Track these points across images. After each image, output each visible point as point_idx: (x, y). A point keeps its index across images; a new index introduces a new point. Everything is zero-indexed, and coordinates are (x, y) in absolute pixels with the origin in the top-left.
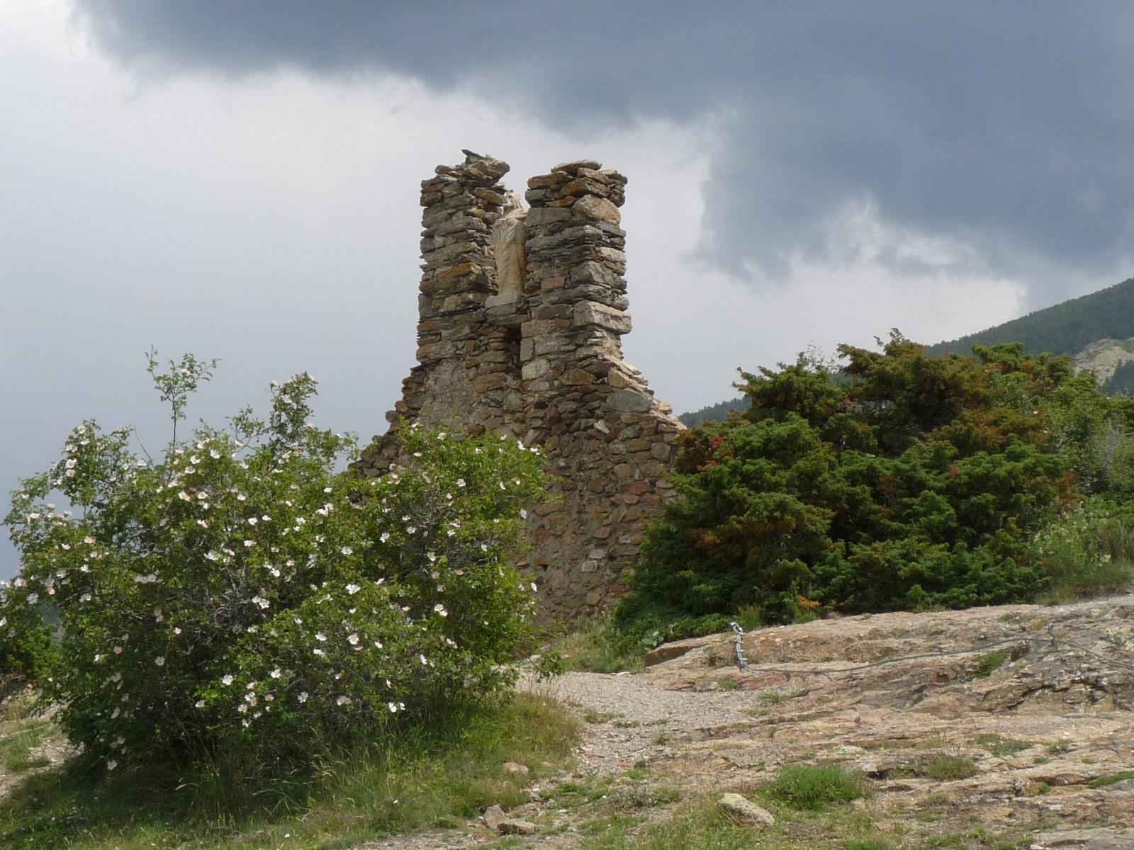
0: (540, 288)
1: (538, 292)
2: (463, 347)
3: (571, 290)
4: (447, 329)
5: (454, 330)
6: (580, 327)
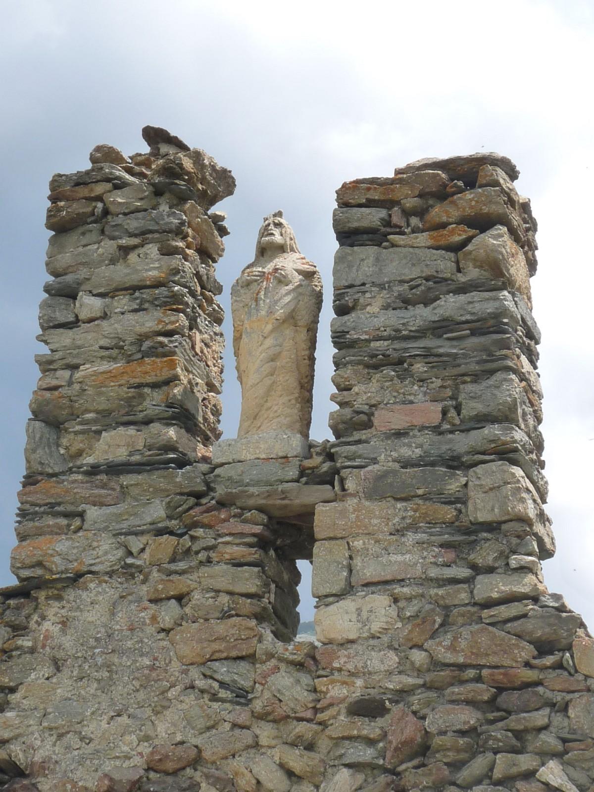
0: (368, 425)
1: (363, 435)
2: (143, 550)
3: (457, 436)
4: (102, 505)
5: (122, 507)
6: (482, 524)
